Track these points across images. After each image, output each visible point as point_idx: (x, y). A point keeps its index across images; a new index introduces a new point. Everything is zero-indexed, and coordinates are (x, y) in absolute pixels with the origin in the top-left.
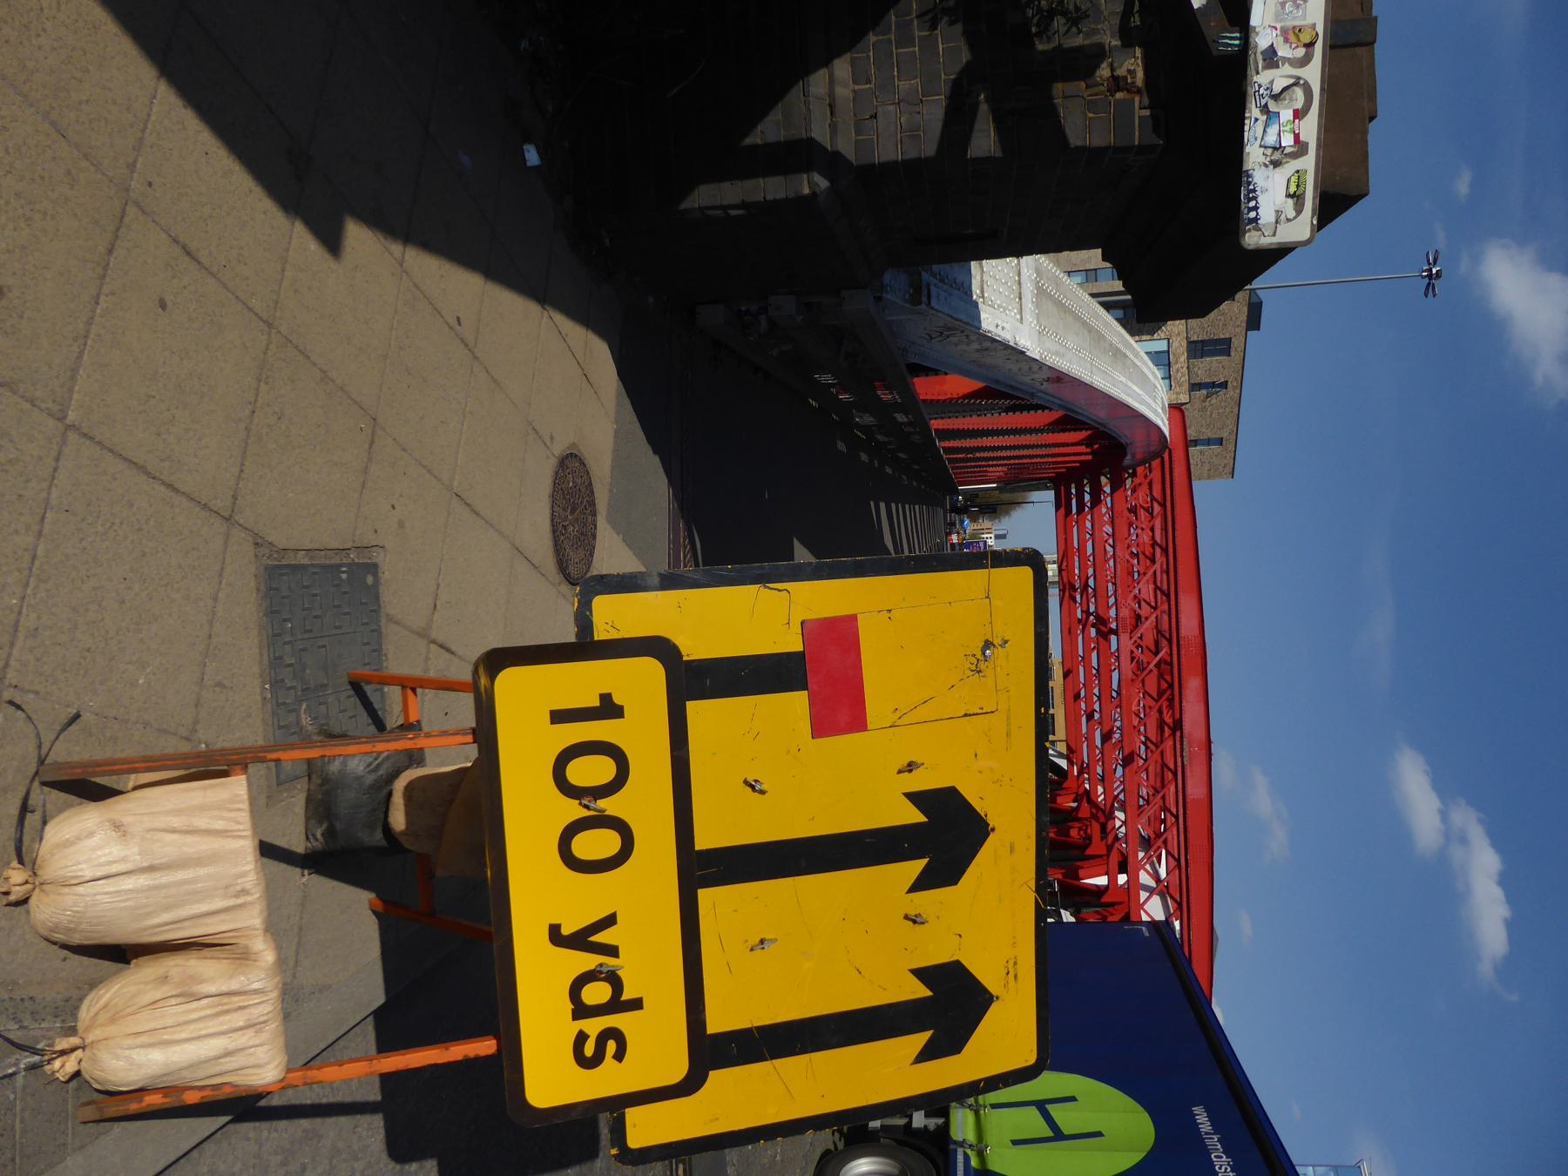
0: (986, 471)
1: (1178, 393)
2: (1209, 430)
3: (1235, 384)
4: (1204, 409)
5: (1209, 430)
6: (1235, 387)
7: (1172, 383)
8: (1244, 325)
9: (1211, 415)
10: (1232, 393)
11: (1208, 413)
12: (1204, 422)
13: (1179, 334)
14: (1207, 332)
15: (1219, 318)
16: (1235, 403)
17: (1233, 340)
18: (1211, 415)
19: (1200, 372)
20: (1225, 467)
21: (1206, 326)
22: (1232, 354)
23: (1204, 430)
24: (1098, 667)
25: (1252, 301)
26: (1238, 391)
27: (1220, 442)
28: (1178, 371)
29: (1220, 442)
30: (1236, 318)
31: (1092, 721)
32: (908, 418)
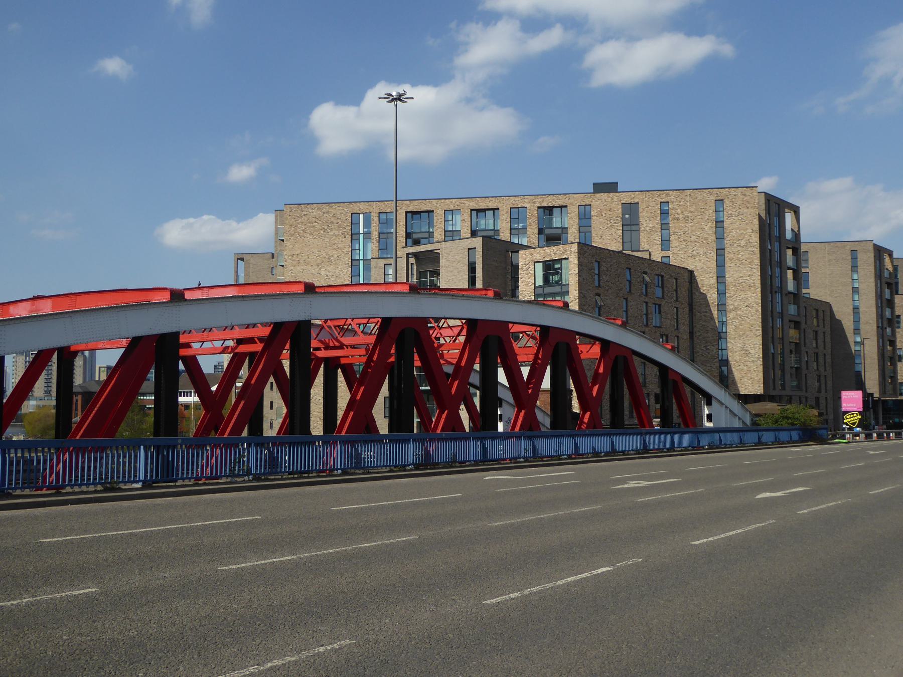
0: (371, 451)
1: (571, 252)
2: (706, 212)
3: (664, 195)
4: (686, 219)
5: (706, 212)
6: (667, 195)
7: (564, 257)
8: (611, 195)
9: (692, 212)
10: (672, 197)
11: (690, 214)
12: (698, 217)
13: (532, 255)
14: (615, 223)
15: (604, 215)
16: (682, 193)
17: (624, 202)
18: (692, 212)
19: (651, 226)
20: (745, 195)
21: (609, 225)
22: (636, 201)
23: (707, 217)
24: (527, 347)
25: (592, 191)
26: (671, 192)
27: (719, 201)
28: (555, 254)
29: (719, 201)
30: (605, 201)
31: (631, 353)
32: (846, 424)
